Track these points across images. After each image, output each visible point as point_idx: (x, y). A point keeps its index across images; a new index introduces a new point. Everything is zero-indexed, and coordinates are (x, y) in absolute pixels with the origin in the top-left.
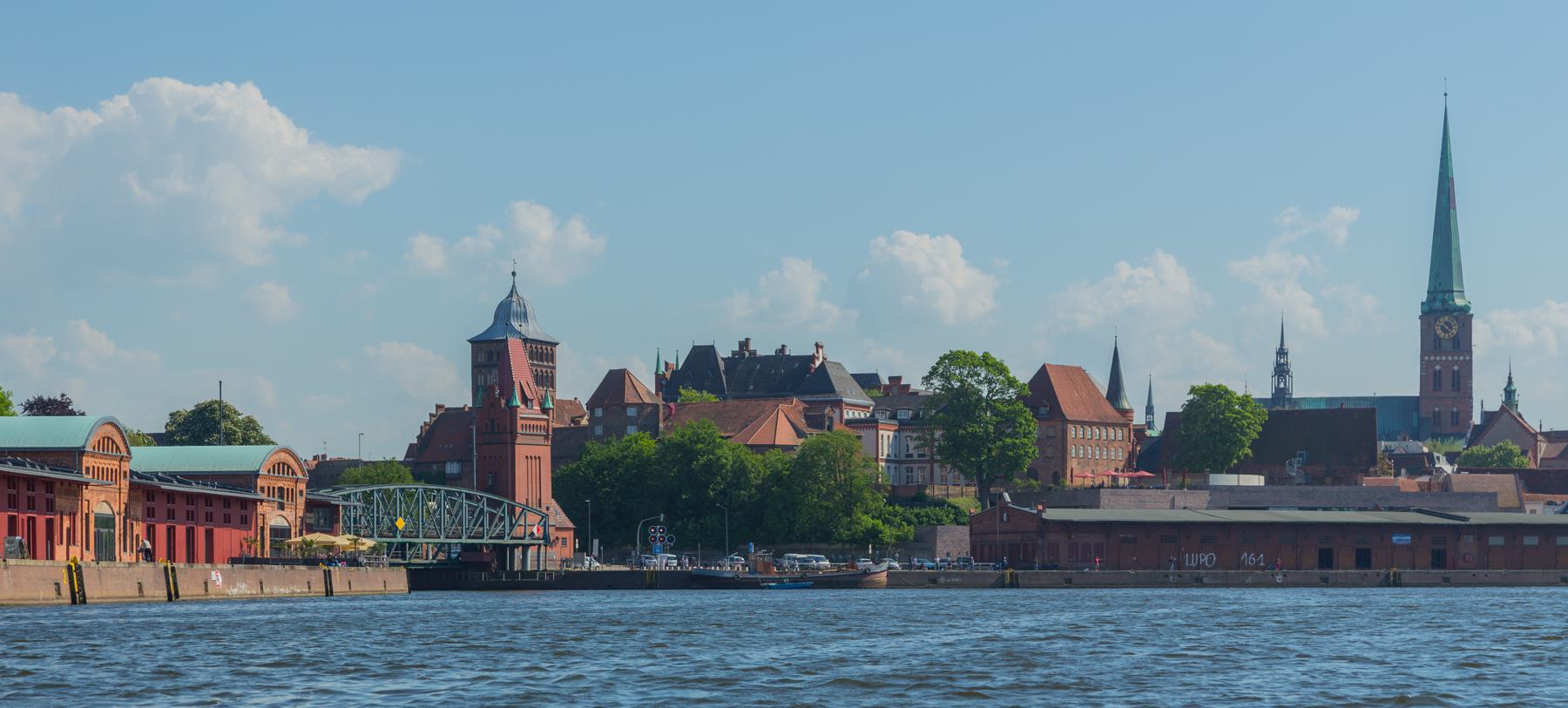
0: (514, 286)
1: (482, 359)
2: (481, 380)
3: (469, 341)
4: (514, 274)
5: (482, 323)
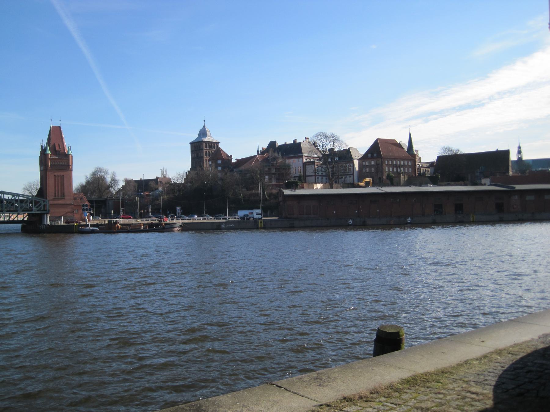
0: (204, 125)
1: (193, 149)
2: (193, 155)
3: (190, 143)
4: (204, 121)
5: (194, 136)
